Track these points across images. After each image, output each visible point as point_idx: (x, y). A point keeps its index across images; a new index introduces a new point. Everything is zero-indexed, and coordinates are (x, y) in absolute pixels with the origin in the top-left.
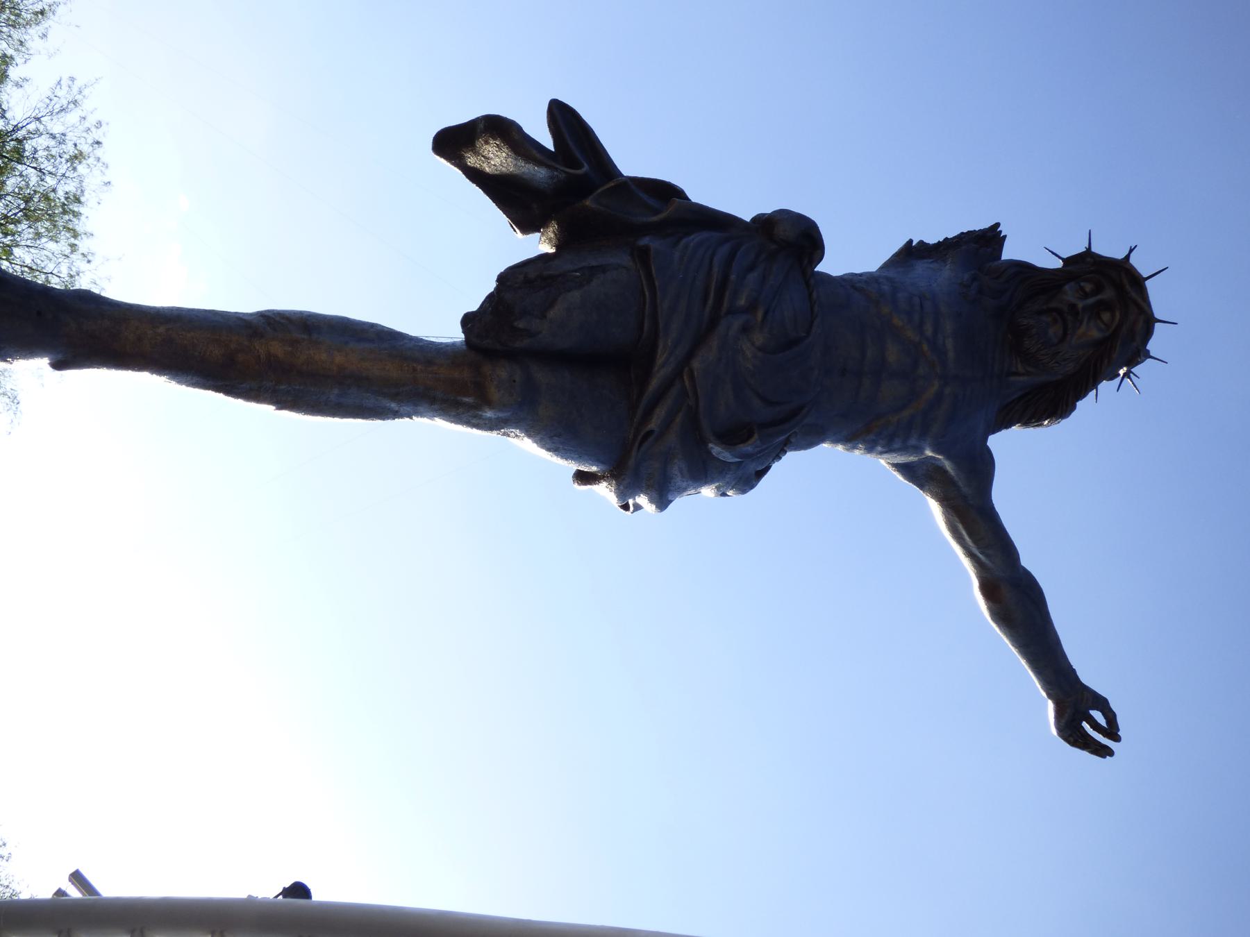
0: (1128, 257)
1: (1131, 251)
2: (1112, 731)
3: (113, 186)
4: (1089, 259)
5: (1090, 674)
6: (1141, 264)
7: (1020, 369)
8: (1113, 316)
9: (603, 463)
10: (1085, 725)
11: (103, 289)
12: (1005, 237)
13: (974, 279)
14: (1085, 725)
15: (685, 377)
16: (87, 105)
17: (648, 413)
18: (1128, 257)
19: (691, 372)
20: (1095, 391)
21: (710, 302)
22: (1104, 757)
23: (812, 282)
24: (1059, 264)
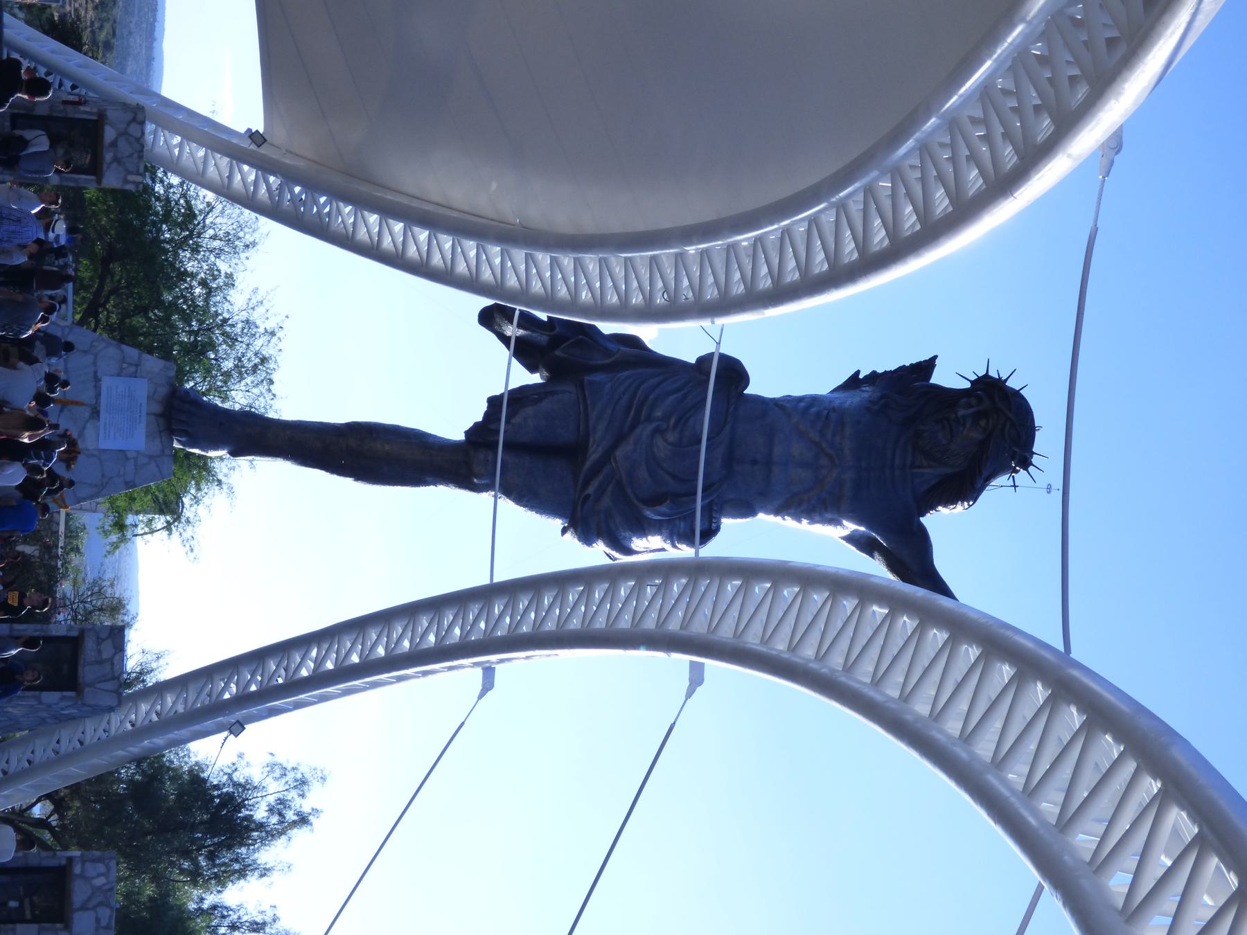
3: (324, 768)
7: (925, 463)
11: (280, 416)
13: (882, 397)
16: (267, 305)
17: (586, 483)
21: (632, 413)
24: (968, 385)
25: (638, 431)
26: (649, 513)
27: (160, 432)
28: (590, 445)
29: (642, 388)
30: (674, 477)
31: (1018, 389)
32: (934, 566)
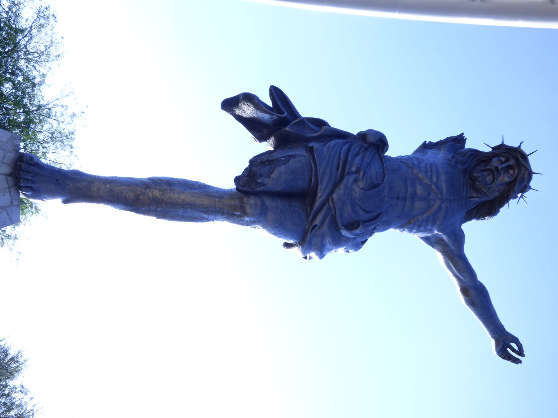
0: (520, 146)
1: (521, 143)
2: (521, 352)
4: (503, 148)
5: (510, 327)
6: (526, 149)
7: (475, 195)
8: (514, 172)
9: (295, 239)
10: (509, 350)
12: (466, 139)
14: (509, 350)
15: (330, 202)
18: (520, 146)
19: (333, 199)
20: (507, 204)
21: (340, 169)
22: (517, 363)
23: (384, 160)
24: (490, 150)
25: (345, 180)
26: (344, 232)
27: (9, 188)
28: (319, 191)
29: (342, 151)
30: (364, 210)
31: (528, 154)
32: (464, 252)
